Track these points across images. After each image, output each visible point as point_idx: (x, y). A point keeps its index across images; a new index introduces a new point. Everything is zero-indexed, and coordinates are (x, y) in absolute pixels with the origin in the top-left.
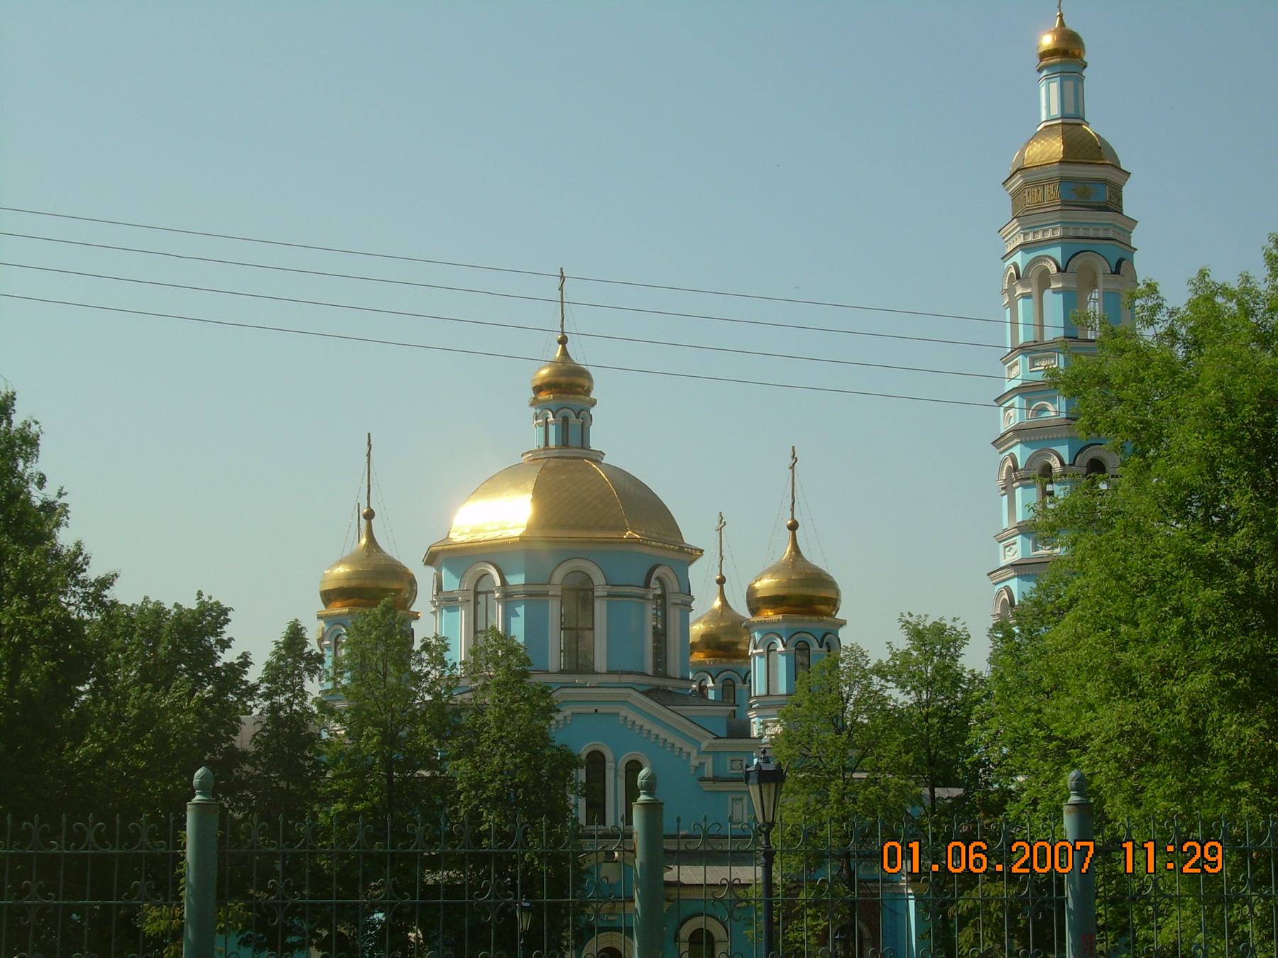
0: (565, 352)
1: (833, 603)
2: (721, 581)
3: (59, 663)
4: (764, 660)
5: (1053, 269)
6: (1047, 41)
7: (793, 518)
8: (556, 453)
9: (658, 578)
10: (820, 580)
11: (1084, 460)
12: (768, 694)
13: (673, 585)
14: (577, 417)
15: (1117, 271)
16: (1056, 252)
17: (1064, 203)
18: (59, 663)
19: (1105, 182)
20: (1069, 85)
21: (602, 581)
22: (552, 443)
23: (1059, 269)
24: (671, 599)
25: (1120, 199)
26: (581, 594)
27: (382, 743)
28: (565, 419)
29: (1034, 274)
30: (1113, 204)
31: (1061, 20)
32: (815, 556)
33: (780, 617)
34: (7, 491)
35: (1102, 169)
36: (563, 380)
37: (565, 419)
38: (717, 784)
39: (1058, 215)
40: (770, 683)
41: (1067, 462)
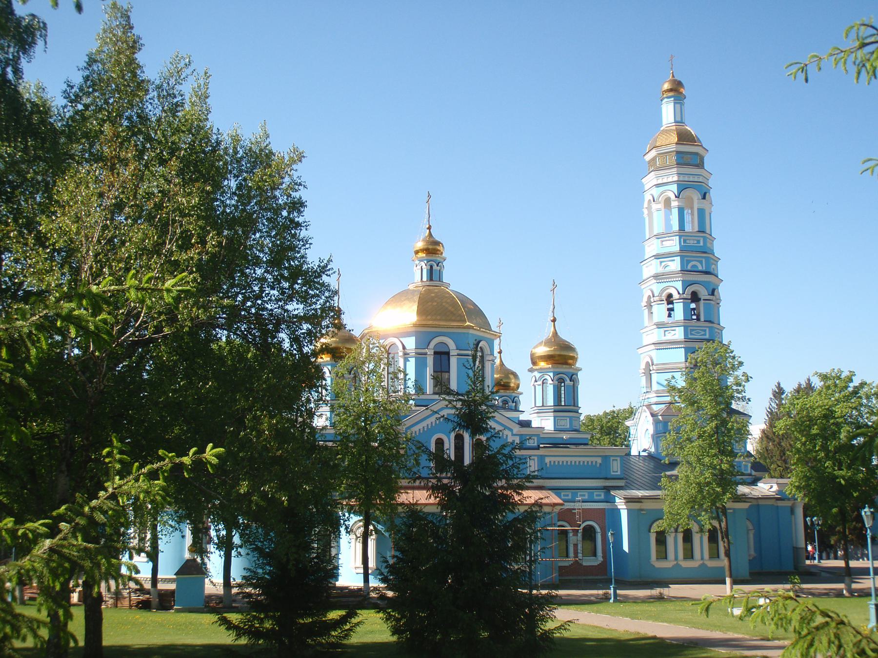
0: (430, 234)
1: (574, 359)
2: (554, 321)
3: (437, 484)
4: (541, 387)
5: (673, 197)
6: (666, 86)
7: (554, 316)
8: (428, 283)
9: (481, 348)
10: (568, 347)
11: (689, 290)
12: (543, 406)
13: (487, 351)
14: (438, 266)
15: (704, 198)
16: (674, 188)
17: (677, 164)
18: (437, 484)
19: (697, 154)
20: (678, 106)
21: (454, 347)
22: (425, 279)
23: (676, 197)
24: (487, 358)
25: (703, 163)
26: (442, 356)
27: (114, 205)
28: (431, 267)
29: (662, 199)
30: (700, 165)
31: (673, 75)
32: (564, 335)
33: (550, 366)
34: (304, 419)
35: (696, 147)
36: (430, 247)
37: (431, 267)
38: (521, 451)
39: (675, 170)
40: (572, 390)
41: (681, 292)
